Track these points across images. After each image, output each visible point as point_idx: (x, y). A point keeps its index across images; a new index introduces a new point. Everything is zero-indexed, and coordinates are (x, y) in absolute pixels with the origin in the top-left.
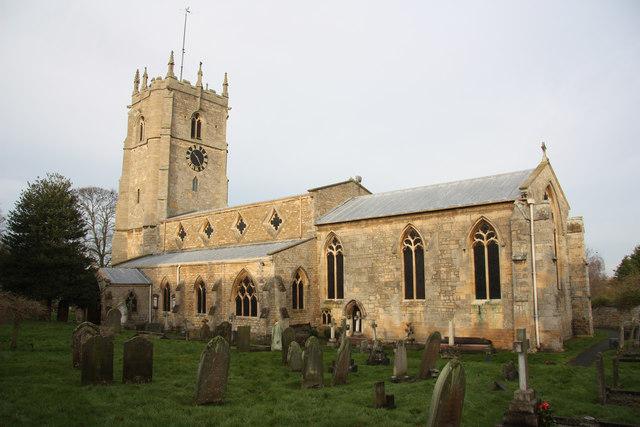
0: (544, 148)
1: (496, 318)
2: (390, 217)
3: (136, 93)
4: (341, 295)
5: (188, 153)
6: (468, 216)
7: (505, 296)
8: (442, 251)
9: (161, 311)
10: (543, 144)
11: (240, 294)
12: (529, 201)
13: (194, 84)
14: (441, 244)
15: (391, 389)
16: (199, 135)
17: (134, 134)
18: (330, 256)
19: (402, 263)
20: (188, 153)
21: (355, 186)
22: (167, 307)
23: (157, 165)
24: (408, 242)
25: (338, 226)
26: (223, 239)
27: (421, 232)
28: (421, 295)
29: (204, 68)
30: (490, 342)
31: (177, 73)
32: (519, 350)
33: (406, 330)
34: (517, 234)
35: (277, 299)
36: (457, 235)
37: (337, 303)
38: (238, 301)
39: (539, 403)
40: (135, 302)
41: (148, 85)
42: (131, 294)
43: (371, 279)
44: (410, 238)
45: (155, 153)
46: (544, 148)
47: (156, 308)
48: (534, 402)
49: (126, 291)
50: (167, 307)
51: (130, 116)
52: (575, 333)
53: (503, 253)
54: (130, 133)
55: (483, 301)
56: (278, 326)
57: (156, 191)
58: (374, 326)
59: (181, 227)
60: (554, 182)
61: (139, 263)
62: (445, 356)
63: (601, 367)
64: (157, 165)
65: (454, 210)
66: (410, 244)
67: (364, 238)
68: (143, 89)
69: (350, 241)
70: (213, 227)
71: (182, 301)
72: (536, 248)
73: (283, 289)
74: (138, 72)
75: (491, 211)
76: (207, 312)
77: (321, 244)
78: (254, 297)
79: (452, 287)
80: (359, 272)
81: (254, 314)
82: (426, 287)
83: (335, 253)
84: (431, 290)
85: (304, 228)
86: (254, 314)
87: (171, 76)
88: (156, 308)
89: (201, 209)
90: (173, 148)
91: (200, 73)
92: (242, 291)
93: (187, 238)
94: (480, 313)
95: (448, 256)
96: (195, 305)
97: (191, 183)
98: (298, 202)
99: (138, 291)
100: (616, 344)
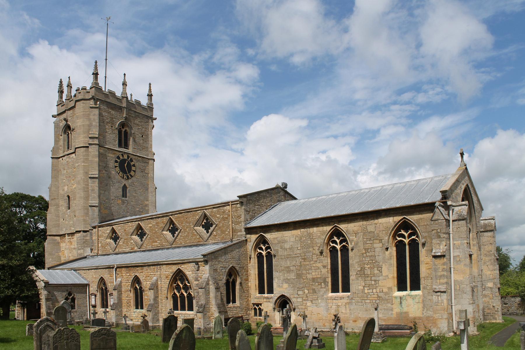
1: (410, 304)
3: (60, 104)
4: (271, 291)
5: (116, 162)
6: (392, 218)
8: (366, 250)
10: (61, 80)
11: (176, 291)
12: (449, 203)
13: (119, 94)
14: (365, 243)
17: (61, 143)
18: (260, 256)
19: (328, 261)
20: (116, 162)
21: (281, 193)
22: (105, 304)
23: (86, 173)
26: (156, 242)
28: (346, 288)
31: (101, 83)
34: (437, 232)
36: (381, 235)
37: (267, 298)
38: (174, 297)
41: (73, 95)
43: (299, 276)
45: (84, 162)
47: (94, 306)
50: (105, 304)
53: (423, 252)
54: (56, 141)
57: (87, 198)
59: (113, 231)
60: (470, 186)
64: (86, 173)
67: (293, 239)
68: (68, 102)
69: (279, 242)
71: (120, 299)
72: (454, 244)
74: (61, 82)
77: (250, 246)
78: (189, 294)
79: (375, 281)
80: (288, 270)
82: (351, 281)
84: (355, 283)
85: (234, 231)
87: (96, 86)
88: (94, 306)
90: (102, 157)
91: (124, 84)
92: (178, 288)
94: (401, 303)
96: (133, 302)
97: (121, 190)
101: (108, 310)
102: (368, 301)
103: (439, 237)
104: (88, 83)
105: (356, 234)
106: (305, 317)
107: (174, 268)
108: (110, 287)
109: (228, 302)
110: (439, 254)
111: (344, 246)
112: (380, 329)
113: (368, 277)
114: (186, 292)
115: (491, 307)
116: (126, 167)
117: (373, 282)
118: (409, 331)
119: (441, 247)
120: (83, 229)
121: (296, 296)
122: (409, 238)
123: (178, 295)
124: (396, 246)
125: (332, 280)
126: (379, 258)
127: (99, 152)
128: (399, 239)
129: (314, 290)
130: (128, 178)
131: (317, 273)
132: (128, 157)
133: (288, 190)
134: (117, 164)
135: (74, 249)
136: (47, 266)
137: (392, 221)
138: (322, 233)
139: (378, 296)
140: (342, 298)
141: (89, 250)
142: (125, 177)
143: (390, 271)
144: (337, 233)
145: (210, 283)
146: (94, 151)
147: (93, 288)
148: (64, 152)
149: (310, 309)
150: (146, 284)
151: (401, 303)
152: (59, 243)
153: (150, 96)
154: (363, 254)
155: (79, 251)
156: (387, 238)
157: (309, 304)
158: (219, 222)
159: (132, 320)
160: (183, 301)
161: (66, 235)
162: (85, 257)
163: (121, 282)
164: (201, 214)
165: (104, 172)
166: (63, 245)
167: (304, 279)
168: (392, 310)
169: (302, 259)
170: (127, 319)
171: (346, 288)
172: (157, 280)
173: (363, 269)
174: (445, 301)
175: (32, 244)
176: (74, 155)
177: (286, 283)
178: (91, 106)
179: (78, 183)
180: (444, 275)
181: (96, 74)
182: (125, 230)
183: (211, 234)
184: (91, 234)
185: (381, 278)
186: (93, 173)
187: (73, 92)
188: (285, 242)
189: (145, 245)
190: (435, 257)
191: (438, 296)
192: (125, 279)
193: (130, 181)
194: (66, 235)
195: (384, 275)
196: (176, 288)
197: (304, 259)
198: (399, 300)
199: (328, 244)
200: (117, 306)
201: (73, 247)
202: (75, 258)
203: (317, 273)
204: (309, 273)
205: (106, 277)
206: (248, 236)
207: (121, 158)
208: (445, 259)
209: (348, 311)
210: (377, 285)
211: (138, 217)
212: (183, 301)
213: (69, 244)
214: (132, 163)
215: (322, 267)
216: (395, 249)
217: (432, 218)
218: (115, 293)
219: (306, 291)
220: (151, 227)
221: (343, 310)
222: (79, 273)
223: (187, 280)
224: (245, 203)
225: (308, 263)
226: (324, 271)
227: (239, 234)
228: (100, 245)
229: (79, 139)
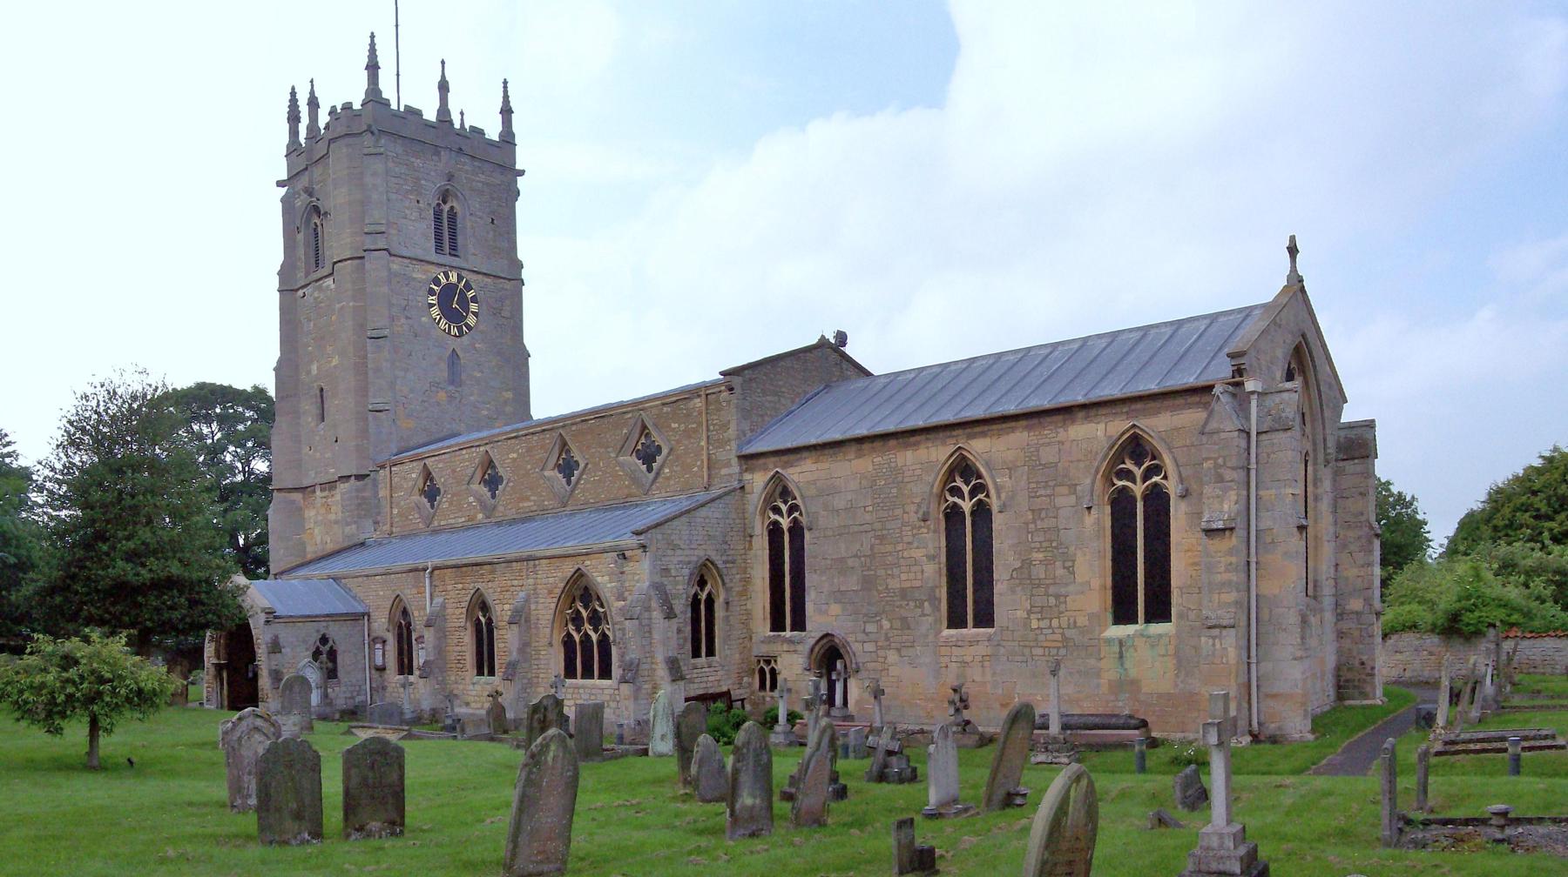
0: (1293, 250)
2: (885, 437)
3: (293, 150)
4: (799, 624)
6: (1101, 426)
7: (1181, 616)
9: (393, 677)
10: (1293, 238)
11: (571, 627)
12: (1250, 386)
13: (430, 115)
14: (1033, 496)
15: (924, 835)
16: (454, 247)
17: (301, 252)
18: (775, 531)
20: (432, 292)
21: (827, 362)
22: (405, 667)
24: (956, 492)
25: (792, 457)
26: (528, 499)
27: (987, 465)
28: (985, 618)
29: (449, 67)
30: (1144, 724)
31: (387, 90)
32: (1213, 739)
33: (952, 702)
34: (1217, 466)
35: (656, 636)
37: (790, 641)
38: (568, 643)
39: (1252, 855)
40: (332, 655)
42: (324, 640)
43: (868, 583)
44: (959, 483)
46: (1293, 250)
47: (382, 669)
48: (1242, 851)
49: (312, 633)
50: (405, 667)
51: (286, 202)
52: (1340, 697)
53: (1179, 514)
55: (1130, 629)
56: (668, 697)
58: (878, 693)
59: (428, 475)
60: (1311, 336)
61: (337, 566)
62: (1042, 758)
63: (1392, 773)
65: (1066, 412)
66: (961, 495)
67: (853, 485)
70: (501, 471)
73: (670, 615)
74: (293, 93)
75: (1157, 413)
76: (417, 673)
78: (604, 635)
79: (1057, 597)
81: (606, 673)
83: (785, 523)
86: (606, 673)
88: (382, 669)
89: (470, 429)
91: (444, 87)
92: (577, 620)
93: (443, 502)
94: (1121, 657)
95: (1051, 523)
97: (444, 366)
98: (698, 403)
99: (336, 632)
100: (1428, 719)
101: (411, 678)
102: (1039, 651)
103: (1220, 479)
105: (1011, 469)
106: (878, 693)
107: (568, 569)
109: (696, 653)
110: (1220, 525)
112: (1065, 727)
113: (1039, 586)
114: (596, 631)
115: (1357, 663)
117: (1052, 601)
118: (1136, 732)
119: (1226, 507)
120: (355, 472)
121: (861, 636)
123: (577, 638)
125: (949, 593)
128: (1120, 483)
129: (904, 619)
130: (461, 334)
131: (912, 576)
132: (460, 278)
133: (849, 350)
134: (433, 300)
135: (336, 522)
136: (273, 569)
137: (1101, 433)
139: (1060, 644)
140: (973, 642)
141: (369, 523)
142: (455, 331)
144: (962, 468)
147: (381, 623)
148: (307, 275)
149: (894, 671)
150: (502, 612)
151: (1121, 653)
152: (300, 509)
153: (507, 112)
154: (1027, 524)
155: (347, 529)
156: (1088, 481)
157: (892, 657)
158: (678, 442)
159: (467, 704)
160: (588, 656)
161: (318, 488)
162: (363, 544)
163: (443, 607)
164: (632, 422)
165: (403, 320)
166: (310, 513)
167: (879, 592)
168: (1098, 676)
169: (877, 537)
170: (457, 702)
171: (985, 618)
172: (527, 600)
173: (1027, 564)
174: (1232, 654)
175: (241, 513)
176: (329, 281)
177: (837, 601)
178: (366, 151)
180: (1230, 582)
181: (373, 67)
182: (454, 471)
183: (658, 474)
184: (375, 484)
185: (1071, 588)
186: (379, 325)
187: (323, 119)
189: (501, 508)
190: (1210, 532)
191: (1214, 638)
192: (453, 601)
194: (318, 488)
195: (1079, 579)
196: (573, 620)
197: (882, 538)
198: (1116, 649)
199: (941, 496)
201: (332, 517)
202: (337, 547)
203: (912, 576)
204: (893, 576)
205: (409, 594)
206: (747, 476)
207: (444, 281)
208: (1234, 539)
209: (989, 677)
210: (1062, 608)
211: (484, 434)
212: (588, 656)
213: (323, 511)
214: (470, 294)
216: (1108, 509)
217: (1206, 423)
219: (886, 624)
220: (514, 460)
221: (975, 673)
222: (344, 587)
223: (599, 598)
224: (738, 390)
225: (889, 548)
227: (724, 471)
228: (395, 511)
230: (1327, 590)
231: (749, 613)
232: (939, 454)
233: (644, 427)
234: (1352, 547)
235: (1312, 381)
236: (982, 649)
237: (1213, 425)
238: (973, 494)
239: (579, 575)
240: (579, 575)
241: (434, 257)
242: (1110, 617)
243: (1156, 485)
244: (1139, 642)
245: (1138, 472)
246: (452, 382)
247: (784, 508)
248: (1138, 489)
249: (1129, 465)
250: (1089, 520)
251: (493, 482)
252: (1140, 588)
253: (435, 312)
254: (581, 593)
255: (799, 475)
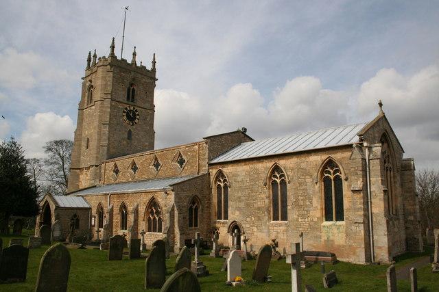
0: (381, 105)
4: (226, 218)
13: (129, 61)
17: (86, 98)
20: (124, 112)
21: (241, 137)
26: (144, 174)
28: (285, 218)
29: (141, 48)
30: (333, 255)
36: (311, 171)
37: (223, 223)
43: (248, 205)
44: (276, 174)
51: (84, 85)
53: (345, 184)
55: (331, 223)
57: (99, 140)
59: (116, 166)
60: (389, 131)
67: (243, 174)
74: (90, 53)
80: (240, 200)
84: (292, 214)
91: (134, 54)
92: (152, 212)
93: (120, 174)
104: (107, 54)
107: (150, 196)
108: (105, 210)
109: (191, 225)
110: (357, 189)
111: (283, 180)
116: (131, 117)
122: (334, 174)
124: (324, 181)
126: (310, 192)
127: (111, 104)
132: (134, 108)
137: (319, 159)
138: (266, 168)
143: (317, 204)
144: (276, 168)
145: (175, 209)
146: (107, 103)
147: (94, 212)
150: (130, 208)
153: (154, 63)
157: (255, 229)
162: (95, 186)
166: (81, 176)
171: (285, 218)
176: (94, 107)
179: (95, 128)
181: (113, 47)
184: (100, 168)
188: (237, 175)
190: (354, 191)
193: (134, 127)
199: (270, 178)
200: (110, 227)
206: (211, 170)
215: (263, 198)
218: (108, 216)
226: (267, 201)
229: (97, 95)
230: (401, 212)
231: (210, 214)
232: (269, 164)
233: (180, 154)
234: (408, 199)
235: (391, 145)
236: (283, 228)
237: (353, 157)
238: (280, 177)
239: (153, 199)
240: (153, 199)
241: (126, 102)
242: (324, 219)
243: (338, 176)
244: (334, 227)
245: (332, 172)
246: (129, 139)
247: (222, 180)
248: (332, 177)
249: (329, 169)
250: (317, 187)
251: (135, 169)
252: (334, 209)
253: (125, 117)
254: (153, 204)
255: (227, 170)
